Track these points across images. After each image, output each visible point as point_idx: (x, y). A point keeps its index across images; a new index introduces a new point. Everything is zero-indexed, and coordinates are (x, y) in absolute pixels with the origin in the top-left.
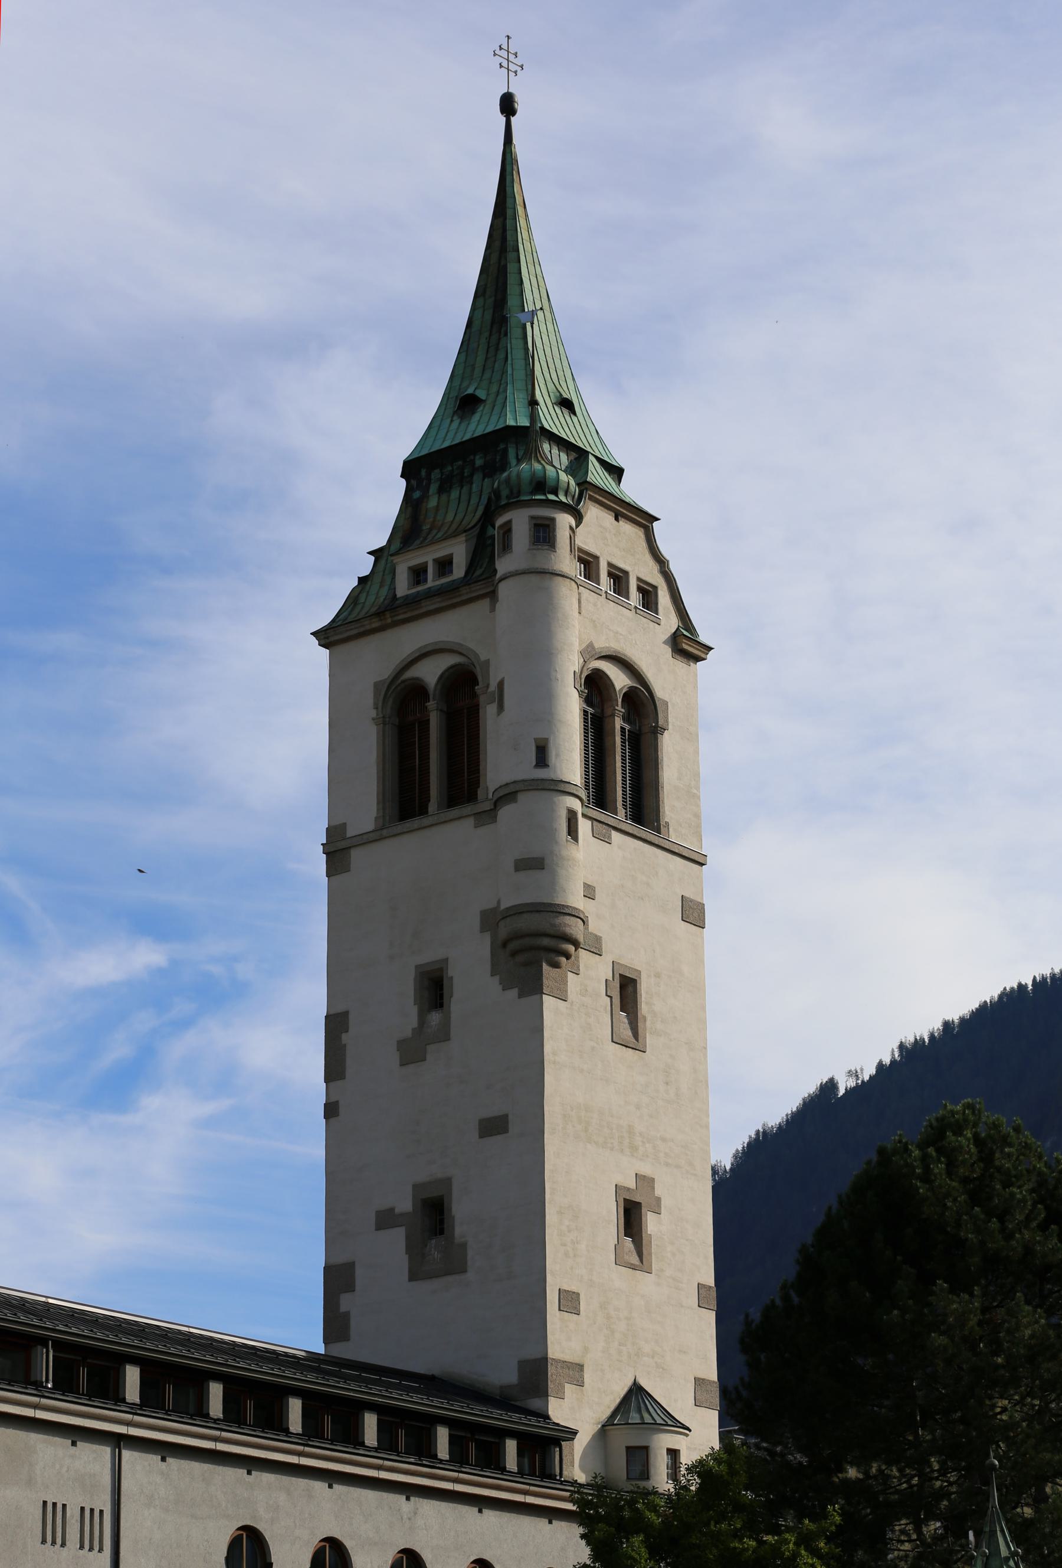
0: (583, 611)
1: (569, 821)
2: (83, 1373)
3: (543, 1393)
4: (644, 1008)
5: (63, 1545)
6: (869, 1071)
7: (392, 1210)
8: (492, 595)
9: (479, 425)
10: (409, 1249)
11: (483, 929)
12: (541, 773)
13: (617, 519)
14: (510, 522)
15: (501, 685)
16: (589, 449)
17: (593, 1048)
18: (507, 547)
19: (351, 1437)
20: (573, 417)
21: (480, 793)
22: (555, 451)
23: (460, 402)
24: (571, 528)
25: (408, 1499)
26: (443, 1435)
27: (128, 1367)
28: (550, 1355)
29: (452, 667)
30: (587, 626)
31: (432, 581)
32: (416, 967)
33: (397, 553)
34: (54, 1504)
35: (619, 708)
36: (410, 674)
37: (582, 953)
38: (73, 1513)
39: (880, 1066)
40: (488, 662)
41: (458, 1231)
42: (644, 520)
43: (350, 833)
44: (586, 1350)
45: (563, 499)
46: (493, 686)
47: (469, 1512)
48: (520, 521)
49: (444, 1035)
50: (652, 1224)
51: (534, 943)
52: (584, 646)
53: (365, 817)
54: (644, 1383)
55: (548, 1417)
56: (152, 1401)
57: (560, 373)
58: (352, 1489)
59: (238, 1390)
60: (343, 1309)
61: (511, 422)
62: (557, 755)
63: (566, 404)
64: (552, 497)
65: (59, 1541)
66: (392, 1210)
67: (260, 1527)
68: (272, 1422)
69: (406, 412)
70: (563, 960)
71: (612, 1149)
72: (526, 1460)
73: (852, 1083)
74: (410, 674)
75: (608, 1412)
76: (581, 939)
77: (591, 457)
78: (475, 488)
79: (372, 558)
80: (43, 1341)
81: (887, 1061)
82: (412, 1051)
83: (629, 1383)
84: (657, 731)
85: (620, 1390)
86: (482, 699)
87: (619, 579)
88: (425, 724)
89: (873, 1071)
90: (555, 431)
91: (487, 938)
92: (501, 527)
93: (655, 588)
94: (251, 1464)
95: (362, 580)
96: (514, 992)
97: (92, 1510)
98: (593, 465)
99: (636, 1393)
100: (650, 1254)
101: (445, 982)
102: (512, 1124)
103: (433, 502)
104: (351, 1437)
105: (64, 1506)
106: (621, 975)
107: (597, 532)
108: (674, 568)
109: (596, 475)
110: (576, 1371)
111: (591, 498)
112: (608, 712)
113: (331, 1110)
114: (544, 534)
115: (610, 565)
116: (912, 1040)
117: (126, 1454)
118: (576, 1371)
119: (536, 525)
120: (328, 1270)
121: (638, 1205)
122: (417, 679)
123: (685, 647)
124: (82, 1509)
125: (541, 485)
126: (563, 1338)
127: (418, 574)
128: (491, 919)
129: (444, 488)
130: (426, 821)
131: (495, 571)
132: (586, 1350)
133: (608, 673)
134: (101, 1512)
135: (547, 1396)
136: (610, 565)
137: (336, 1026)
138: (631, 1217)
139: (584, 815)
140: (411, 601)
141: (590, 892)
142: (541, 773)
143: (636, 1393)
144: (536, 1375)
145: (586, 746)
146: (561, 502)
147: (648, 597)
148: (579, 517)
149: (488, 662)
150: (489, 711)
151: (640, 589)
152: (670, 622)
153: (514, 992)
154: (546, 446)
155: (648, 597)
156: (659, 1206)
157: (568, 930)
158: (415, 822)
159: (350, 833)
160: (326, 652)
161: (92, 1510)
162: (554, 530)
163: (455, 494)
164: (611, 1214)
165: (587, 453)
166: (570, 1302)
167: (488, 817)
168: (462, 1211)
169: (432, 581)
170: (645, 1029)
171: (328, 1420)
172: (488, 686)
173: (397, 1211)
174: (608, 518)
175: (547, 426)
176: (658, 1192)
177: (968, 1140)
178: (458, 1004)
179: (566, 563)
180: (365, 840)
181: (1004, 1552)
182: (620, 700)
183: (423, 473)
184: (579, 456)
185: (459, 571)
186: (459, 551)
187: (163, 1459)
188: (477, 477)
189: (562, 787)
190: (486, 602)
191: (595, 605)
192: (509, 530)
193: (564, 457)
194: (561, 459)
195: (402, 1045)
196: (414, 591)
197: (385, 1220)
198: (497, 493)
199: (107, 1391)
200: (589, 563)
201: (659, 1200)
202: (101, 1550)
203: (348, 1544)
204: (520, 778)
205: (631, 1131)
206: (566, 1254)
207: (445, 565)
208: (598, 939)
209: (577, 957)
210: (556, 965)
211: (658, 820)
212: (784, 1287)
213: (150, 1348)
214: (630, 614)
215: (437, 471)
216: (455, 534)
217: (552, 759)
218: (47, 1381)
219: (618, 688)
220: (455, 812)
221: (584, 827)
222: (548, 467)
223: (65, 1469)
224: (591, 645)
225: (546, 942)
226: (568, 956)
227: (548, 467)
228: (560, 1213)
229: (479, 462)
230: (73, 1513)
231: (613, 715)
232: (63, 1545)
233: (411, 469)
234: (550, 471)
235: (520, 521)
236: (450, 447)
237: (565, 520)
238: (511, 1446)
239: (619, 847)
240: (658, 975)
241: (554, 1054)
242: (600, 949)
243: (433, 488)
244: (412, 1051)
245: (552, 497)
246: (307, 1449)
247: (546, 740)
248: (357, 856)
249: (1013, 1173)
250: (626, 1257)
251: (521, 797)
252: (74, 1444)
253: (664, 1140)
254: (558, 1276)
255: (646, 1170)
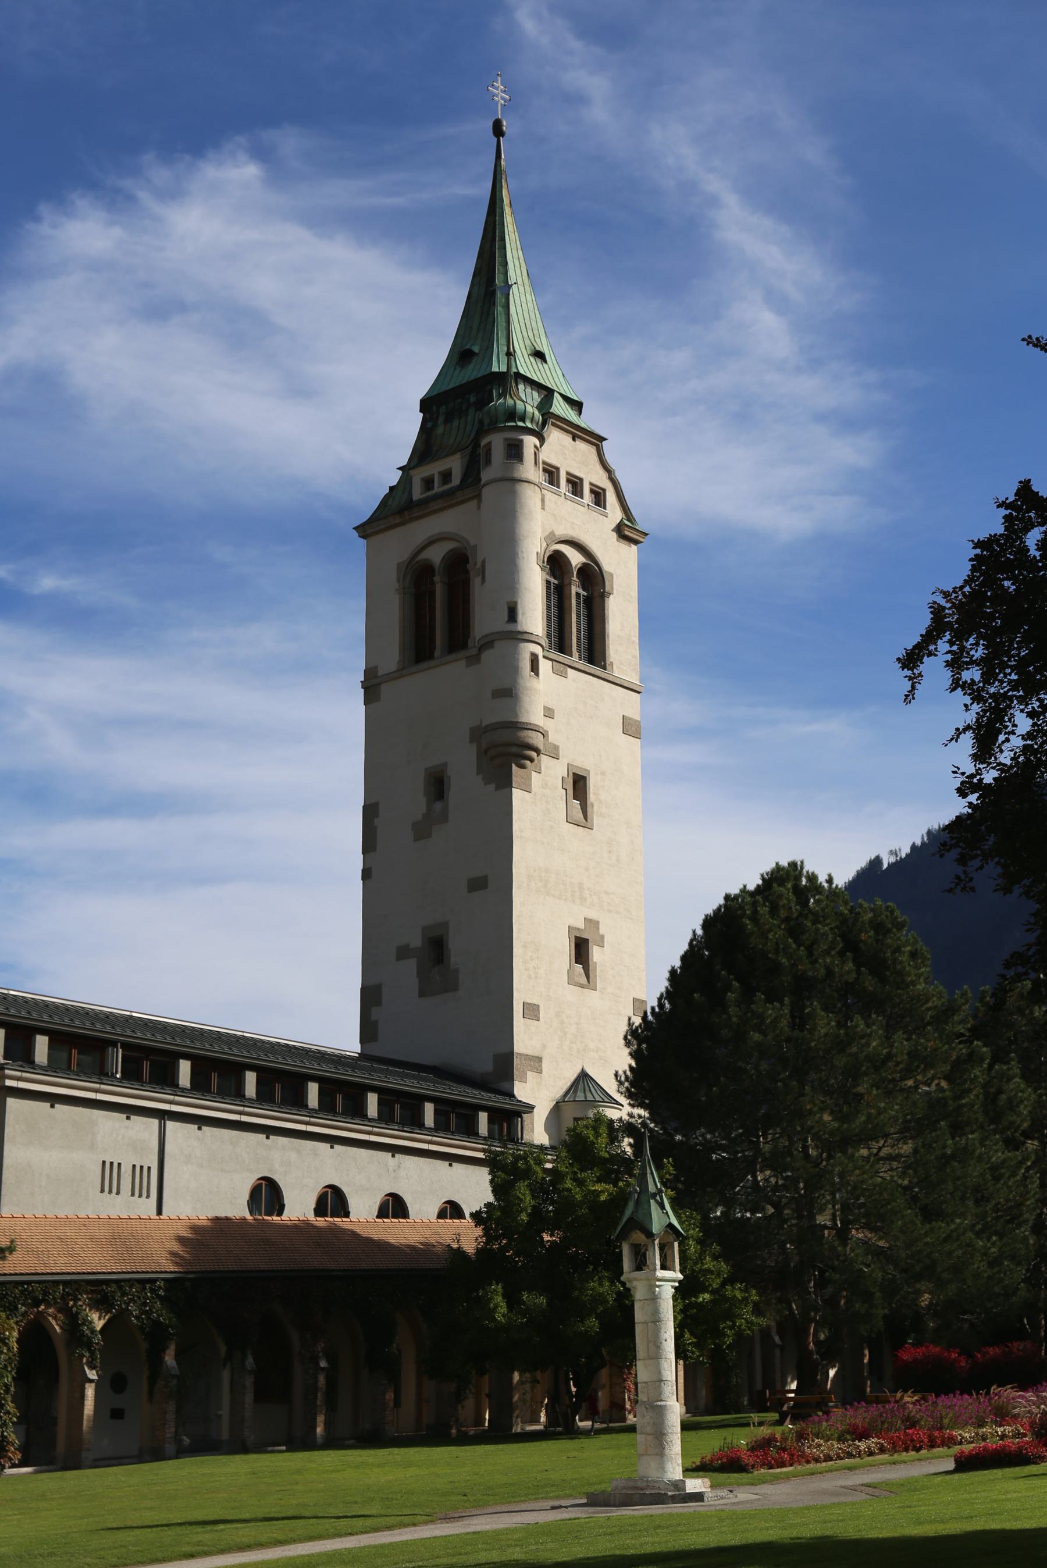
0: (546, 507)
1: (532, 661)
2: (146, 1066)
3: (511, 1079)
4: (592, 797)
5: (118, 1193)
6: (905, 851)
7: (407, 946)
8: (478, 497)
9: (472, 372)
10: (419, 974)
11: (471, 742)
12: (510, 627)
13: (574, 440)
14: (490, 443)
15: (484, 562)
16: (555, 388)
17: (551, 827)
18: (488, 462)
19: (357, 1111)
20: (545, 365)
21: (470, 643)
22: (529, 390)
23: (462, 354)
24: (535, 446)
25: (393, 1156)
26: (429, 1109)
27: (181, 1061)
28: (516, 1050)
29: (451, 551)
30: (545, 519)
31: (437, 489)
32: (426, 769)
33: (413, 468)
34: (112, 1163)
35: (575, 578)
36: (423, 556)
37: (543, 757)
38: (127, 1170)
39: (914, 847)
40: (475, 547)
41: (452, 960)
42: (596, 440)
43: (380, 673)
44: (544, 1046)
45: (529, 425)
46: (479, 565)
47: (443, 1165)
48: (497, 442)
49: (444, 818)
50: (596, 954)
51: (506, 750)
52: (547, 533)
53: (391, 661)
54: (590, 1072)
55: (513, 1096)
56: (200, 1086)
57: (536, 332)
58: (349, 1148)
59: (268, 1077)
60: (373, 1018)
61: (495, 369)
62: (523, 614)
63: (539, 355)
64: (520, 424)
65: (114, 1190)
66: (407, 946)
67: (276, 1177)
68: (296, 1101)
69: (424, 365)
70: (528, 762)
71: (566, 900)
72: (496, 1127)
73: (893, 859)
74: (423, 556)
75: (562, 1092)
76: (541, 747)
77: (556, 394)
78: (470, 418)
79: (400, 472)
80: (114, 1044)
81: (918, 843)
82: (422, 831)
83: (578, 1070)
84: (603, 596)
85: (571, 1075)
86: (472, 573)
87: (575, 485)
88: (432, 594)
89: (908, 851)
90: (529, 375)
91: (474, 746)
92: (485, 446)
93: (604, 490)
94: (269, 1131)
95: (391, 488)
96: (492, 786)
97: (142, 1167)
98: (557, 400)
99: (583, 1077)
100: (595, 976)
101: (445, 779)
102: (491, 882)
103: (440, 430)
104: (357, 1111)
105: (119, 1164)
106: (574, 774)
107: (559, 449)
108: (619, 475)
109: (559, 407)
110: (536, 1062)
111: (553, 424)
112: (566, 581)
113: (366, 874)
114: (515, 452)
115: (568, 473)
116: (937, 827)
117: (170, 1125)
118: (536, 1062)
119: (509, 445)
120: (363, 990)
121: (586, 941)
122: (427, 560)
123: (627, 533)
124: (134, 1166)
125: (512, 414)
126: (525, 1038)
127: (428, 483)
128: (477, 734)
129: (448, 420)
130: (432, 663)
131: (480, 480)
132: (544, 1046)
133: (566, 553)
134: (149, 1168)
135: (513, 1080)
136: (568, 473)
137: (370, 812)
138: (581, 950)
139: (544, 657)
140: (423, 503)
141: (549, 713)
142: (510, 627)
143: (583, 1077)
144: (503, 1068)
145: (549, 607)
146: (527, 428)
147: (599, 497)
148: (542, 440)
149: (475, 547)
150: (476, 581)
151: (592, 491)
152: (615, 514)
153: (492, 786)
154: (521, 387)
155: (599, 497)
156: (603, 941)
157: (530, 741)
158: (425, 665)
159: (380, 673)
160: (363, 542)
161: (142, 1167)
162: (522, 448)
163: (455, 423)
164: (565, 948)
165: (553, 391)
166: (532, 1011)
167: (474, 660)
168: (455, 945)
169: (437, 489)
170: (593, 813)
171: (339, 1098)
172: (476, 564)
173: (411, 947)
174: (567, 439)
175: (522, 371)
176: (601, 932)
177: (788, 890)
178: (454, 795)
179: (530, 470)
180: (391, 677)
181: (652, 1189)
182: (575, 573)
183: (434, 408)
184: (547, 393)
185: (456, 480)
186: (455, 464)
187: (199, 1128)
188: (471, 411)
189: (526, 637)
190: (475, 502)
191: (556, 503)
192: (490, 449)
193: (535, 394)
194: (536, 397)
195: (415, 826)
196: (424, 495)
197: (403, 953)
198: (481, 422)
199: (166, 1079)
200: (551, 473)
201: (602, 937)
202: (148, 1196)
203: (345, 1189)
204: (496, 630)
205: (581, 886)
206: (529, 977)
207: (446, 476)
208: (556, 748)
209: (539, 761)
210: (523, 767)
211: (605, 661)
212: (660, 999)
213: (199, 1048)
214: (584, 510)
215: (444, 407)
216: (454, 453)
217: (520, 617)
218: (117, 1072)
219: (574, 565)
220: (452, 656)
221: (544, 665)
222: (519, 402)
223: (120, 1137)
224: (552, 533)
225: (514, 750)
226: (532, 760)
227: (519, 402)
228: (524, 946)
229: (472, 399)
230: (127, 1170)
231: (570, 584)
232: (118, 1193)
233: (426, 405)
234: (520, 405)
235: (497, 442)
236: (453, 389)
237: (530, 442)
238: (483, 1117)
239: (574, 681)
240: (603, 773)
241: (521, 831)
242: (558, 754)
243: (441, 419)
244: (422, 831)
245: (520, 424)
246: (312, 1120)
247: (516, 603)
248: (385, 689)
249: (821, 914)
250: (577, 979)
251: (497, 644)
252: (128, 1118)
253: (606, 893)
254: (522, 992)
255: (593, 915)
